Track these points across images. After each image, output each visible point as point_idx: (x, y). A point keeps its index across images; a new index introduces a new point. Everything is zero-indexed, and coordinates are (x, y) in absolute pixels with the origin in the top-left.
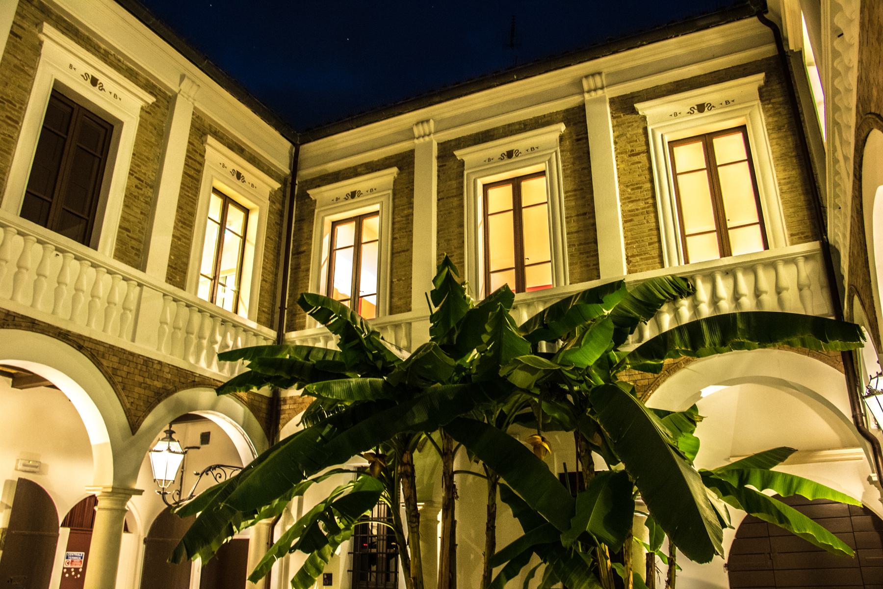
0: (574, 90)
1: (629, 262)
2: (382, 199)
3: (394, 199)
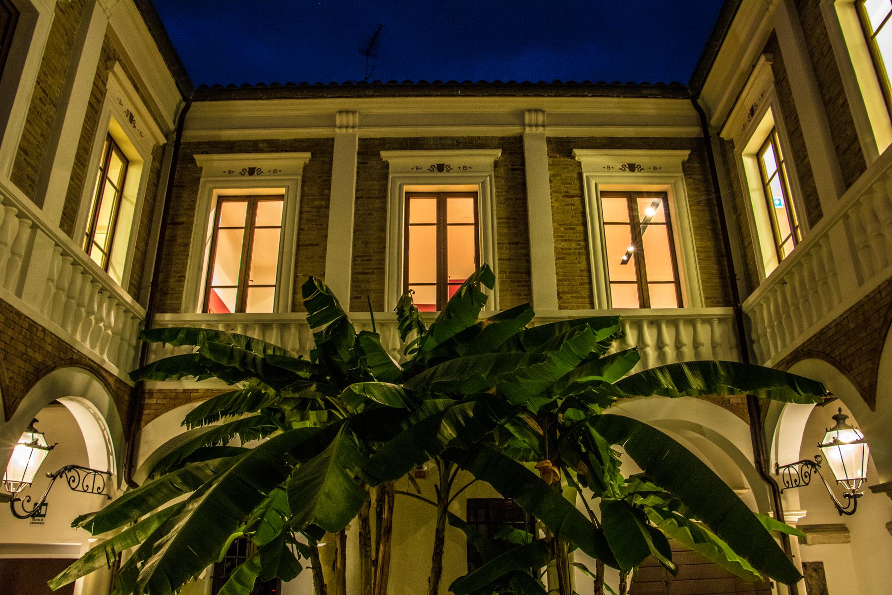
1: (560, 298)
2: (287, 184)
3: (303, 186)
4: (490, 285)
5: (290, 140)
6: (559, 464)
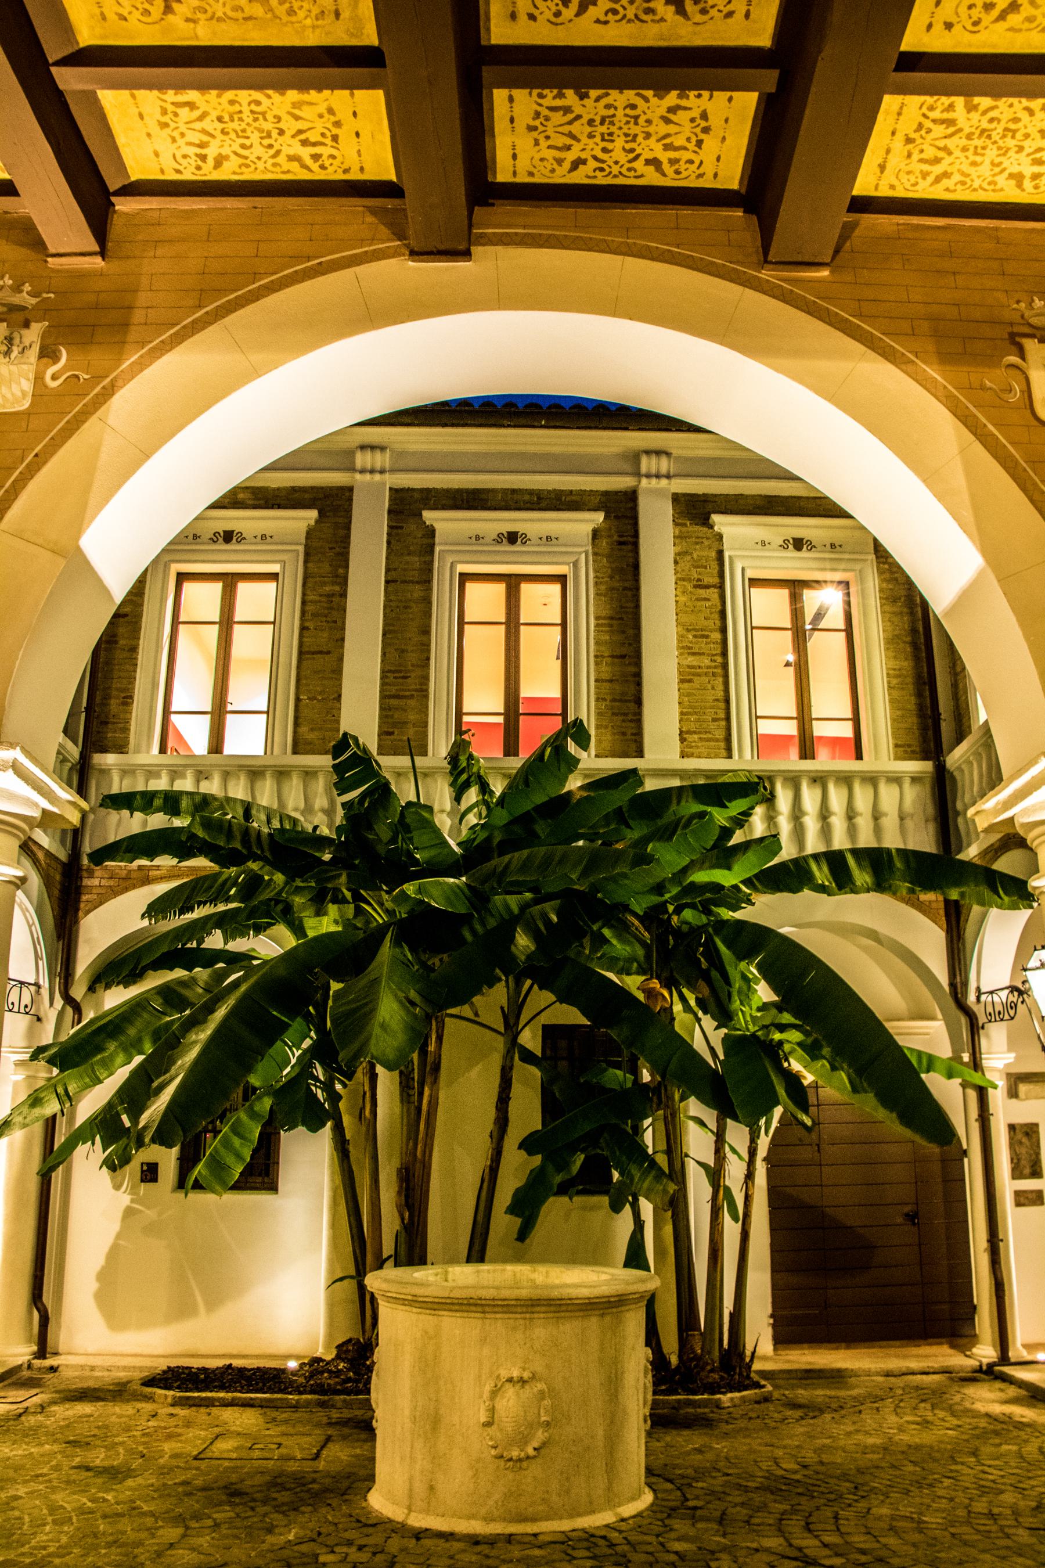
0: (627, 467)
1: (682, 740)
3: (306, 562)
4: (584, 745)
5: (285, 489)
6: (670, 983)
